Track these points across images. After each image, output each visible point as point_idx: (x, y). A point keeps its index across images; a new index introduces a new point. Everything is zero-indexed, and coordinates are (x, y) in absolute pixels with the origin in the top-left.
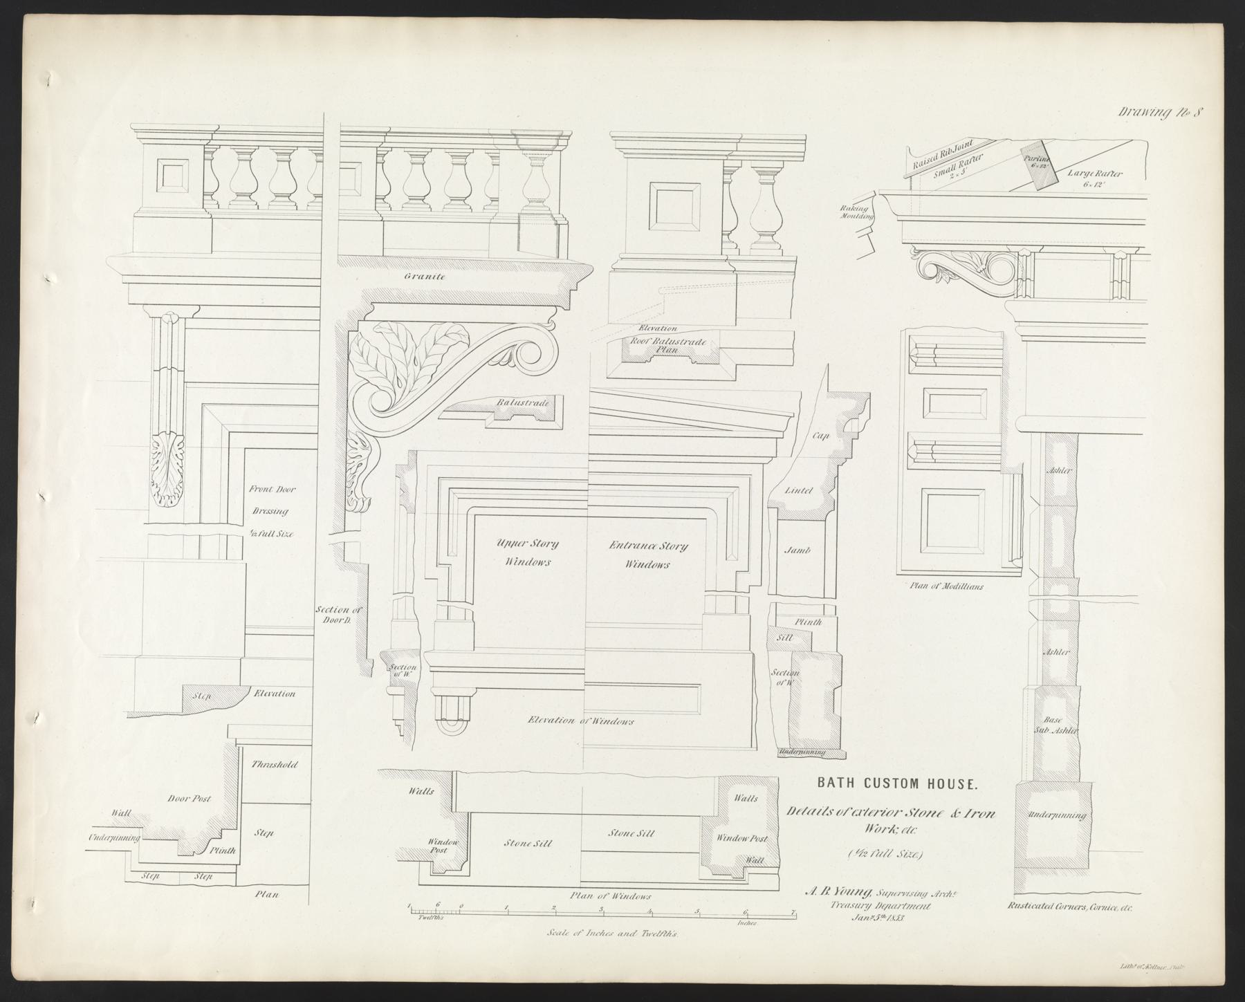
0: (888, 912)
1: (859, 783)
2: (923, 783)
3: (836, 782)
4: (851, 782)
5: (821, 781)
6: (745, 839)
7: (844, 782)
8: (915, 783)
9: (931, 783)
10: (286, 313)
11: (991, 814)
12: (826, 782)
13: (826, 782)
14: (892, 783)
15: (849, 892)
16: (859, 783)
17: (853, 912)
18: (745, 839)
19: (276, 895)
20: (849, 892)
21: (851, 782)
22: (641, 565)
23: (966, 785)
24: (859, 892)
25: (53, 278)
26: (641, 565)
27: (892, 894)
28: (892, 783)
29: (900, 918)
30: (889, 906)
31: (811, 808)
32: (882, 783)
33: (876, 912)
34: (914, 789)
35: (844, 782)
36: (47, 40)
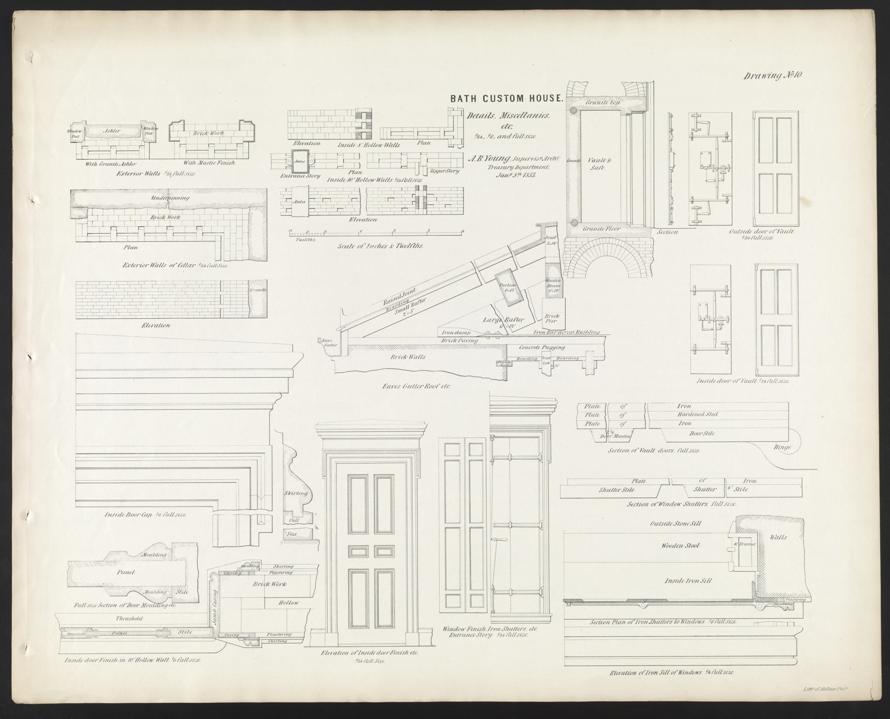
0: (523, 171)
1: (479, 99)
2: (526, 98)
3: (464, 98)
4: (474, 98)
5: (453, 98)
6: (679, 504)
7: (469, 98)
8: (520, 98)
9: (532, 98)
10: (334, 511)
11: (284, 585)
12: (457, 99)
13: (457, 99)
14: (504, 98)
15: (495, 159)
16: (479, 99)
17: (498, 172)
18: (679, 504)
19: (168, 326)
20: (495, 159)
21: (474, 98)
22: (668, 504)
23: (555, 98)
24: (502, 158)
25: (37, 199)
26: (668, 504)
27: (523, 159)
28: (504, 98)
29: (533, 175)
30: (523, 168)
31: (481, 113)
32: (497, 98)
33: (514, 171)
34: (520, 103)
35: (469, 98)
36: (25, 22)
